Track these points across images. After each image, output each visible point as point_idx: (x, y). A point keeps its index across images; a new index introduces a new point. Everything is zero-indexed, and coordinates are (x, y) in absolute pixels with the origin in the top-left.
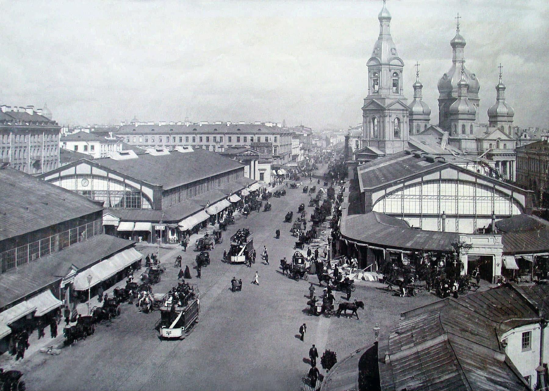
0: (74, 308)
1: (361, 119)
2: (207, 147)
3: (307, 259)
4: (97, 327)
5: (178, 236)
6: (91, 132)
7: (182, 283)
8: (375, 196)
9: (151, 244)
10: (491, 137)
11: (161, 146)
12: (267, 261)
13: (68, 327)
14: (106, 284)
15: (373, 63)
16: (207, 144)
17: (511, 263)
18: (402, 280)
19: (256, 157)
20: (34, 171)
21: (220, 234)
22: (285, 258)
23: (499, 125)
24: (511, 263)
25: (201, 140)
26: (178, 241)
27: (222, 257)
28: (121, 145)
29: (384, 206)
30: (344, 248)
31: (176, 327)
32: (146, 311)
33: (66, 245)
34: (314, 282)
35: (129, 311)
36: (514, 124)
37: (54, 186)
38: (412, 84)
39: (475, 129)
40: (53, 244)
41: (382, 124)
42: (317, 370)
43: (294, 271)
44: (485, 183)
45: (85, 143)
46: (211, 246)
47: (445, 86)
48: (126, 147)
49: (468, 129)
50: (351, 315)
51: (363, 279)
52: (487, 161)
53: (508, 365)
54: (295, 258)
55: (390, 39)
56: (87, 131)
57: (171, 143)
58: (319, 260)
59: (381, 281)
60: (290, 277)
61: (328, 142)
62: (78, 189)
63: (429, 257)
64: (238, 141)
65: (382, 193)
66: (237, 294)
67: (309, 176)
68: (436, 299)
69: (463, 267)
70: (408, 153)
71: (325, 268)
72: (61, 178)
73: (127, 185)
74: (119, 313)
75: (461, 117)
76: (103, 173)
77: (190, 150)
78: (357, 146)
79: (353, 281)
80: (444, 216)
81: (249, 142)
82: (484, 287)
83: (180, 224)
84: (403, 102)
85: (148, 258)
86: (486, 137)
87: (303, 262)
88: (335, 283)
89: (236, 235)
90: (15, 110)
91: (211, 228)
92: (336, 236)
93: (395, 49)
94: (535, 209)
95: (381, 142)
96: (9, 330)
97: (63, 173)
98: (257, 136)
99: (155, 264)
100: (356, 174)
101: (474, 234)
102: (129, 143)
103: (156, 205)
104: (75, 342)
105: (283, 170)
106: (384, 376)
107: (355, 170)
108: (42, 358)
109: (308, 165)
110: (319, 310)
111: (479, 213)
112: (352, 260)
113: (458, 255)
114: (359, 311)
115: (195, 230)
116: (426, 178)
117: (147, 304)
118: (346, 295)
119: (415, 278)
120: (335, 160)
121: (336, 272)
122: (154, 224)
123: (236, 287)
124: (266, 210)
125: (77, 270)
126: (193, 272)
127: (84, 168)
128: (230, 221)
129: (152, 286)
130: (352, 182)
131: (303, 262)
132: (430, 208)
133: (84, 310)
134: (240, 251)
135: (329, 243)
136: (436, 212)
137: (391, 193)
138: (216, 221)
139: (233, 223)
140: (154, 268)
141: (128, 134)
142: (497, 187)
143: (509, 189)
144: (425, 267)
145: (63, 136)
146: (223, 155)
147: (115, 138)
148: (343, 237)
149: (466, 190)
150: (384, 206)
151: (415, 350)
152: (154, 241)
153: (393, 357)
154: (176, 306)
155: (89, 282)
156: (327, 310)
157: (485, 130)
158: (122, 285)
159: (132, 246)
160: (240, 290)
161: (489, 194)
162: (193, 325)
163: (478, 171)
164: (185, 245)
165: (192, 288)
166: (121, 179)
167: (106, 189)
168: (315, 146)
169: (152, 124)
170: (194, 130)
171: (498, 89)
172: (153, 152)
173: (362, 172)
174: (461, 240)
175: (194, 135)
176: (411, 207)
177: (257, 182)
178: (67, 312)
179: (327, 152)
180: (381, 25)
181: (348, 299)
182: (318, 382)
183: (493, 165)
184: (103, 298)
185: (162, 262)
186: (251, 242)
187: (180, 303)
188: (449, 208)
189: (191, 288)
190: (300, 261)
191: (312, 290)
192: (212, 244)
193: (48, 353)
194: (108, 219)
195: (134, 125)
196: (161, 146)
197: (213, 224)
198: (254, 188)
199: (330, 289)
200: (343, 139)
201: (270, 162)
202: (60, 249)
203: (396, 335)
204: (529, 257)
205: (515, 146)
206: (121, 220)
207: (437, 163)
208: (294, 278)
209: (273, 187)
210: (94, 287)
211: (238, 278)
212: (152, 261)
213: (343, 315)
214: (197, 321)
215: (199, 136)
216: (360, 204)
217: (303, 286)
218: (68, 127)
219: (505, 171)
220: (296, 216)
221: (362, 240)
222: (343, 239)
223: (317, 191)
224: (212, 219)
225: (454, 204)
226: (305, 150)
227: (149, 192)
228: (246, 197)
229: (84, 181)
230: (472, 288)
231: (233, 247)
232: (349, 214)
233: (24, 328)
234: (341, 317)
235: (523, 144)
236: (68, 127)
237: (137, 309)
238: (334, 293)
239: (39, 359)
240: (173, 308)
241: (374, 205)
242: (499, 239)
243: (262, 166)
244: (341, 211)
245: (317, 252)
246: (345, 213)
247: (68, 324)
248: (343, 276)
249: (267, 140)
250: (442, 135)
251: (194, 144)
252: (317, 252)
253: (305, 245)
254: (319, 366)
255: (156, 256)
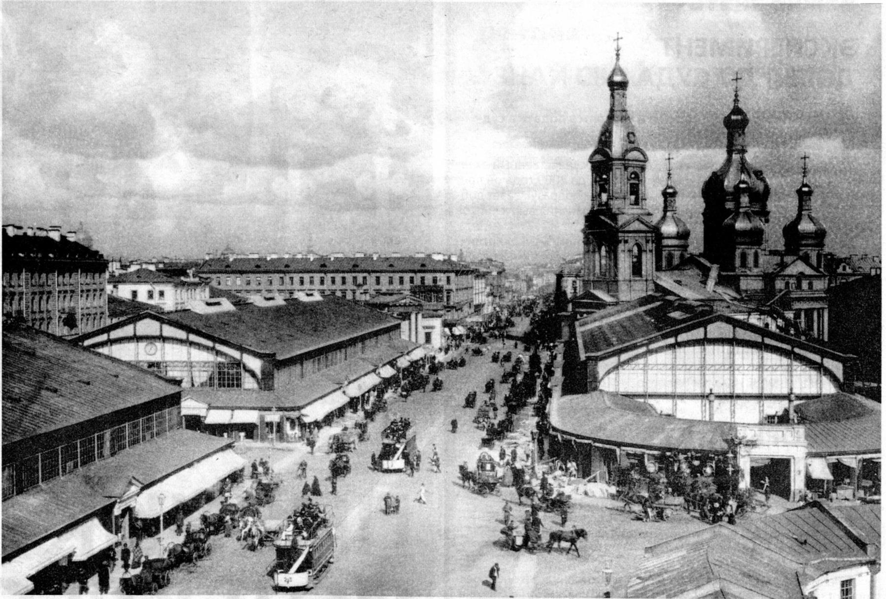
0: (137, 545)
1: (580, 247)
2: (344, 292)
3: (499, 465)
4: (176, 575)
5: (301, 430)
6: (158, 270)
7: (307, 503)
8: (603, 367)
10: (789, 271)
11: (270, 291)
12: (438, 466)
13: (127, 576)
14: (188, 508)
15: (598, 157)
16: (343, 287)
17: (821, 470)
21: (365, 425)
22: (465, 463)
24: (821, 470)
25: (344, 283)
28: (207, 290)
29: (617, 380)
30: (559, 448)
31: (300, 570)
32: (252, 548)
34: (509, 499)
35: (226, 548)
36: (826, 250)
37: (99, 354)
38: (662, 188)
40: (101, 447)
41: (613, 254)
43: (478, 482)
44: (779, 345)
46: (352, 446)
48: (214, 293)
49: (751, 260)
50: (568, 551)
51: (586, 493)
54: (481, 466)
55: (625, 118)
56: (152, 268)
58: (518, 465)
59: (613, 497)
60: (474, 492)
61: (529, 281)
62: (140, 359)
64: (391, 282)
66: (393, 519)
67: (502, 336)
69: (743, 476)
71: (527, 478)
73: (218, 353)
76: (181, 334)
77: (317, 297)
78: (575, 289)
79: (569, 497)
80: (712, 398)
81: (407, 285)
82: (777, 506)
83: (303, 411)
84: (646, 219)
85: (254, 467)
86: (779, 272)
87: (493, 468)
88: (544, 499)
89: (389, 428)
90: (30, 233)
91: (352, 418)
92: (544, 430)
93: (633, 133)
97: (114, 334)
98: (420, 275)
99: (266, 473)
100: (573, 334)
101: (761, 424)
102: (220, 287)
105: (460, 328)
109: (499, 319)
110: (519, 541)
111: (767, 391)
112: (569, 465)
113: (735, 457)
114: (580, 543)
115: (329, 419)
116: (682, 337)
117: (253, 537)
118: (559, 519)
119: (667, 492)
120: (542, 311)
121: (544, 484)
122: (263, 413)
123: (391, 507)
124: (434, 390)
125: (141, 486)
126: (325, 487)
128: (380, 406)
129: (261, 509)
133: (156, 548)
134: (396, 453)
135: (533, 439)
137: (628, 362)
138: (359, 407)
140: (265, 480)
143: (815, 353)
145: (112, 276)
146: (367, 304)
147: (197, 280)
148: (555, 429)
149: (746, 356)
150: (617, 380)
152: (263, 439)
154: (299, 538)
155: (161, 504)
156: (529, 544)
157: (777, 259)
158: (212, 509)
159: (229, 446)
160: (397, 513)
161: (785, 361)
163: (767, 325)
164: (311, 444)
165: (324, 511)
167: (185, 359)
169: (256, 256)
170: (323, 266)
172: (258, 300)
173: (583, 329)
174: (740, 435)
175: (323, 275)
176: (659, 382)
177: (420, 346)
178: (126, 553)
179: (528, 300)
180: (612, 96)
183: (790, 315)
184: (184, 528)
185: (276, 471)
186: (414, 438)
187: (305, 534)
188: (718, 383)
189: (322, 509)
190: (488, 467)
191: (506, 510)
192: (353, 442)
194: (190, 406)
195: (228, 258)
196: (270, 291)
197: (355, 411)
198: (417, 355)
199: (535, 509)
200: (553, 279)
201: (440, 316)
203: (639, 581)
205: (826, 286)
206: (210, 407)
208: (480, 492)
209: (446, 353)
210: (168, 513)
212: (260, 469)
213: (557, 550)
214: (332, 560)
215: (330, 275)
217: (493, 505)
218: (120, 261)
219: (810, 327)
221: (583, 434)
222: (554, 433)
223: (513, 359)
224: (353, 404)
225: (727, 377)
226: (495, 296)
228: (404, 370)
229: (149, 347)
230: (758, 509)
231: (386, 446)
234: (553, 552)
236: (120, 261)
238: (541, 515)
240: (294, 542)
241: (602, 379)
242: (801, 430)
244: (550, 390)
247: (127, 571)
248: (555, 489)
249: (435, 280)
250: (709, 269)
251: (322, 287)
253: (497, 443)
255: (266, 462)
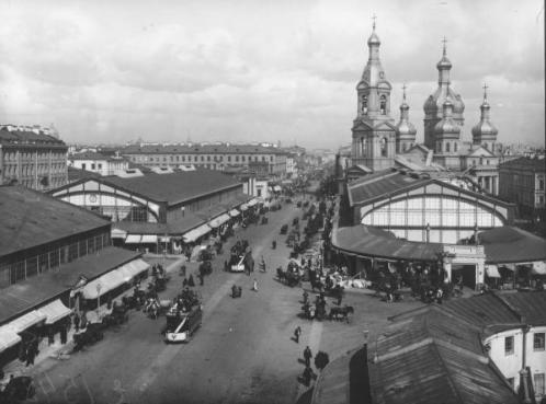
1: (351, 140)
2: (209, 165)
4: (108, 334)
8: (364, 210)
9: (157, 256)
15: (362, 87)
17: (493, 271)
18: (389, 286)
19: (253, 175)
20: (42, 187)
23: (483, 143)
24: (493, 271)
26: (182, 252)
27: (223, 266)
29: (372, 220)
30: (335, 258)
31: (181, 331)
33: (75, 257)
35: (138, 317)
39: (459, 147)
40: (63, 256)
42: (311, 370)
43: (288, 278)
45: (92, 162)
47: (431, 108)
49: (452, 148)
50: (341, 319)
52: (470, 177)
53: (492, 368)
54: (291, 267)
55: (379, 64)
56: (95, 151)
57: (175, 162)
58: (312, 269)
60: (285, 284)
63: (414, 266)
64: (237, 160)
65: (370, 207)
66: (237, 301)
68: (420, 304)
70: (394, 170)
72: (69, 194)
74: (127, 319)
75: (445, 135)
76: (111, 190)
77: (193, 168)
81: (247, 161)
82: (467, 294)
85: (154, 268)
87: (297, 271)
88: (328, 289)
90: (21, 129)
91: (212, 241)
92: (328, 247)
94: (516, 221)
95: (368, 160)
96: (19, 338)
97: (71, 190)
101: (457, 244)
103: (161, 218)
104: (85, 347)
106: (374, 380)
107: (345, 187)
108: (52, 363)
109: (301, 182)
110: (312, 314)
115: (199, 241)
118: (337, 301)
121: (328, 279)
126: (197, 281)
127: (92, 185)
128: (230, 233)
130: (342, 197)
131: (297, 271)
132: (415, 220)
133: (93, 317)
136: (420, 224)
137: (379, 207)
139: (232, 235)
140: (160, 277)
141: (134, 153)
142: (480, 201)
144: (414, 275)
145: (71, 155)
149: (450, 204)
151: (401, 351)
152: (160, 252)
153: (382, 358)
156: (320, 315)
157: (469, 147)
158: (130, 293)
161: (472, 207)
162: (195, 331)
164: (188, 255)
166: (128, 196)
168: (308, 164)
170: (197, 150)
171: (482, 108)
172: (157, 170)
176: (397, 220)
180: (371, 51)
181: (339, 304)
182: (312, 381)
183: (476, 180)
188: (433, 220)
191: (305, 296)
193: (59, 360)
198: (252, 203)
199: (322, 295)
200: (334, 158)
202: (70, 260)
204: (512, 267)
206: (128, 234)
207: (424, 179)
211: (238, 285)
216: (350, 217)
217: (298, 292)
220: (291, 228)
223: (310, 205)
224: (214, 231)
227: (155, 208)
232: (340, 226)
233: (28, 345)
235: (506, 160)
237: (145, 315)
238: (326, 298)
239: (45, 366)
242: (482, 249)
243: (260, 183)
245: (310, 261)
246: (335, 226)
249: (263, 158)
250: (427, 153)
252: (310, 261)
254: (313, 366)
